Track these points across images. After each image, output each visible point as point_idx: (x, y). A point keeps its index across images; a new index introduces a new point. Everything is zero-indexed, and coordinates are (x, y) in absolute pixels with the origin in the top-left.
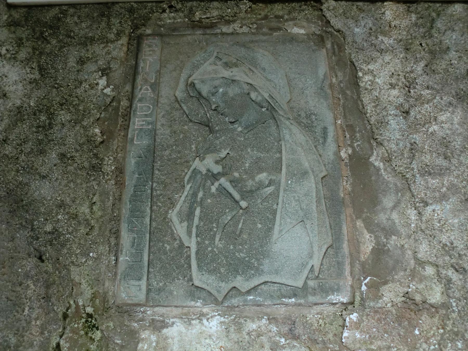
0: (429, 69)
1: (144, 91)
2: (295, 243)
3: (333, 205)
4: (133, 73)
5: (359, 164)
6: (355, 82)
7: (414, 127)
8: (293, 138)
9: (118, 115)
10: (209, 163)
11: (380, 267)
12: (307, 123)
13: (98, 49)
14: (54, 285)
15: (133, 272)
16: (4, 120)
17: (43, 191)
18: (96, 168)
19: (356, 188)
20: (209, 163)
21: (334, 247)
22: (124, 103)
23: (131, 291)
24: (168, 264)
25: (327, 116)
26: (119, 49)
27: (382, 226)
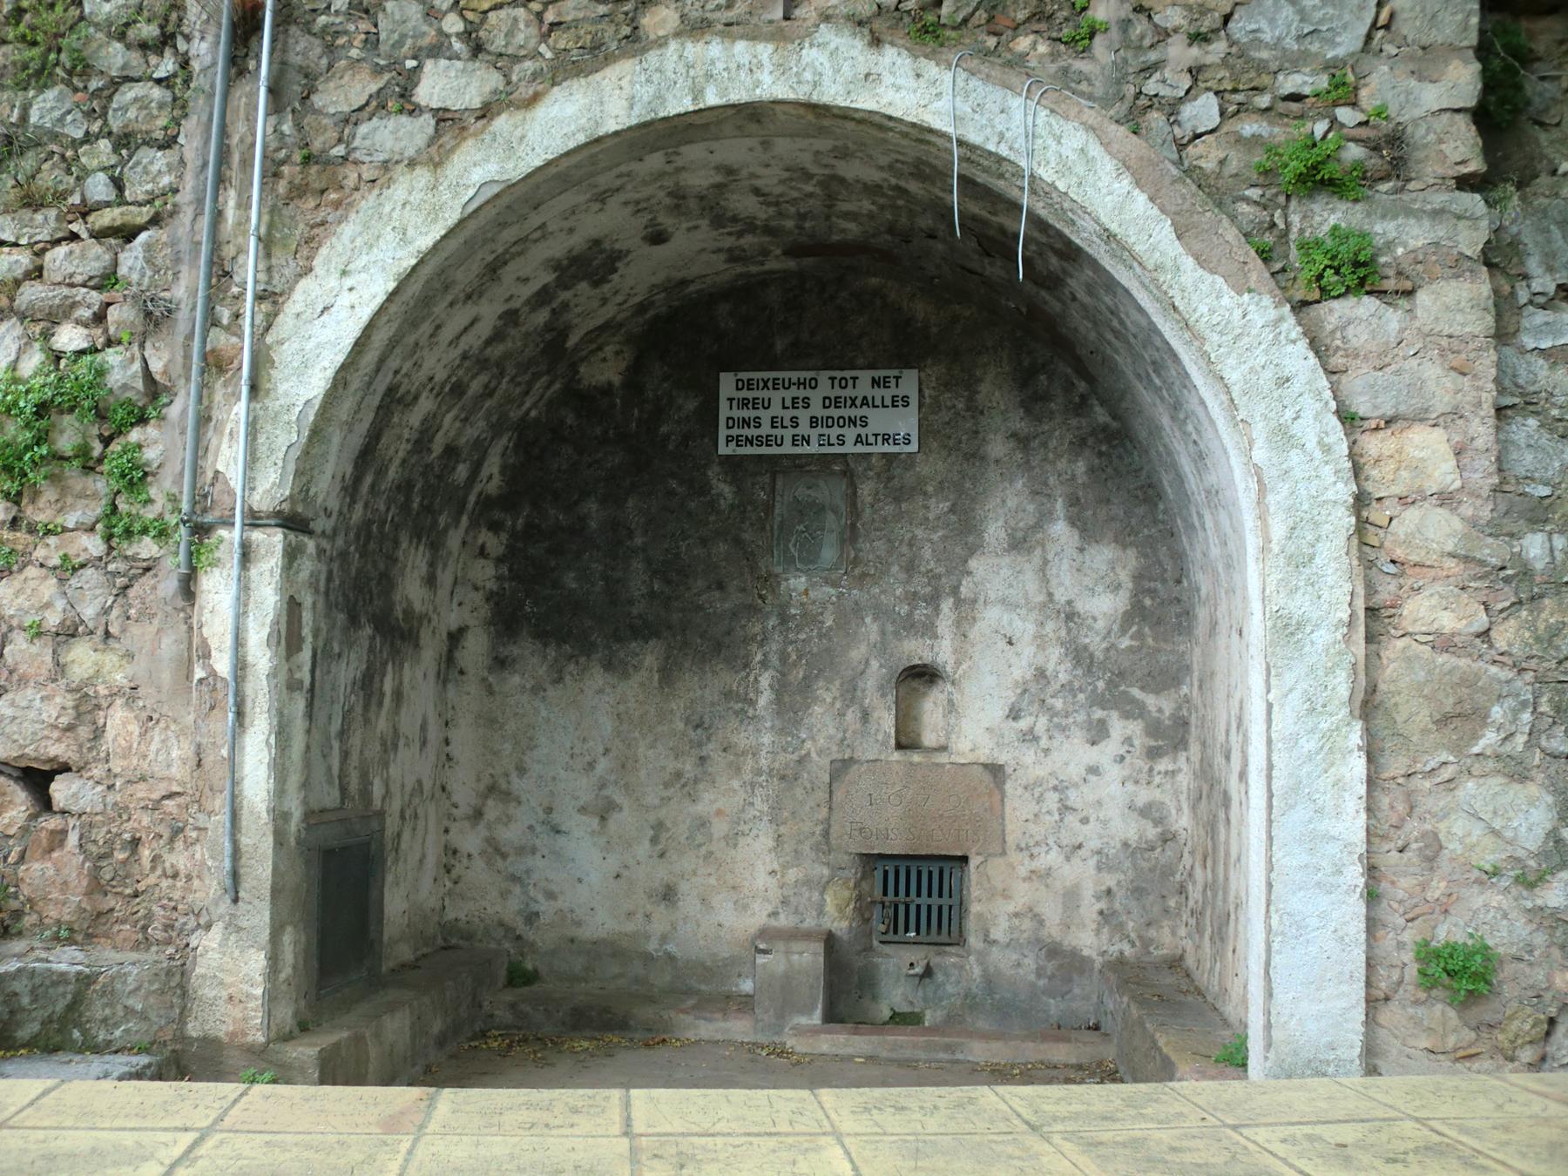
0: (886, 487)
1: (778, 498)
2: (828, 554)
3: (842, 542)
4: (773, 490)
5: (853, 526)
6: (855, 493)
7: (875, 512)
8: (831, 517)
9: (769, 508)
10: (801, 528)
11: (856, 562)
12: (835, 511)
13: (759, 479)
14: (753, 568)
15: (779, 563)
16: (1453, 510)
17: (746, 536)
18: (763, 529)
19: (851, 535)
20: (801, 528)
21: (841, 556)
22: (374, 103)
23: (778, 570)
24: (790, 561)
25: (843, 507)
26: (767, 479)
27: (1548, 877)
